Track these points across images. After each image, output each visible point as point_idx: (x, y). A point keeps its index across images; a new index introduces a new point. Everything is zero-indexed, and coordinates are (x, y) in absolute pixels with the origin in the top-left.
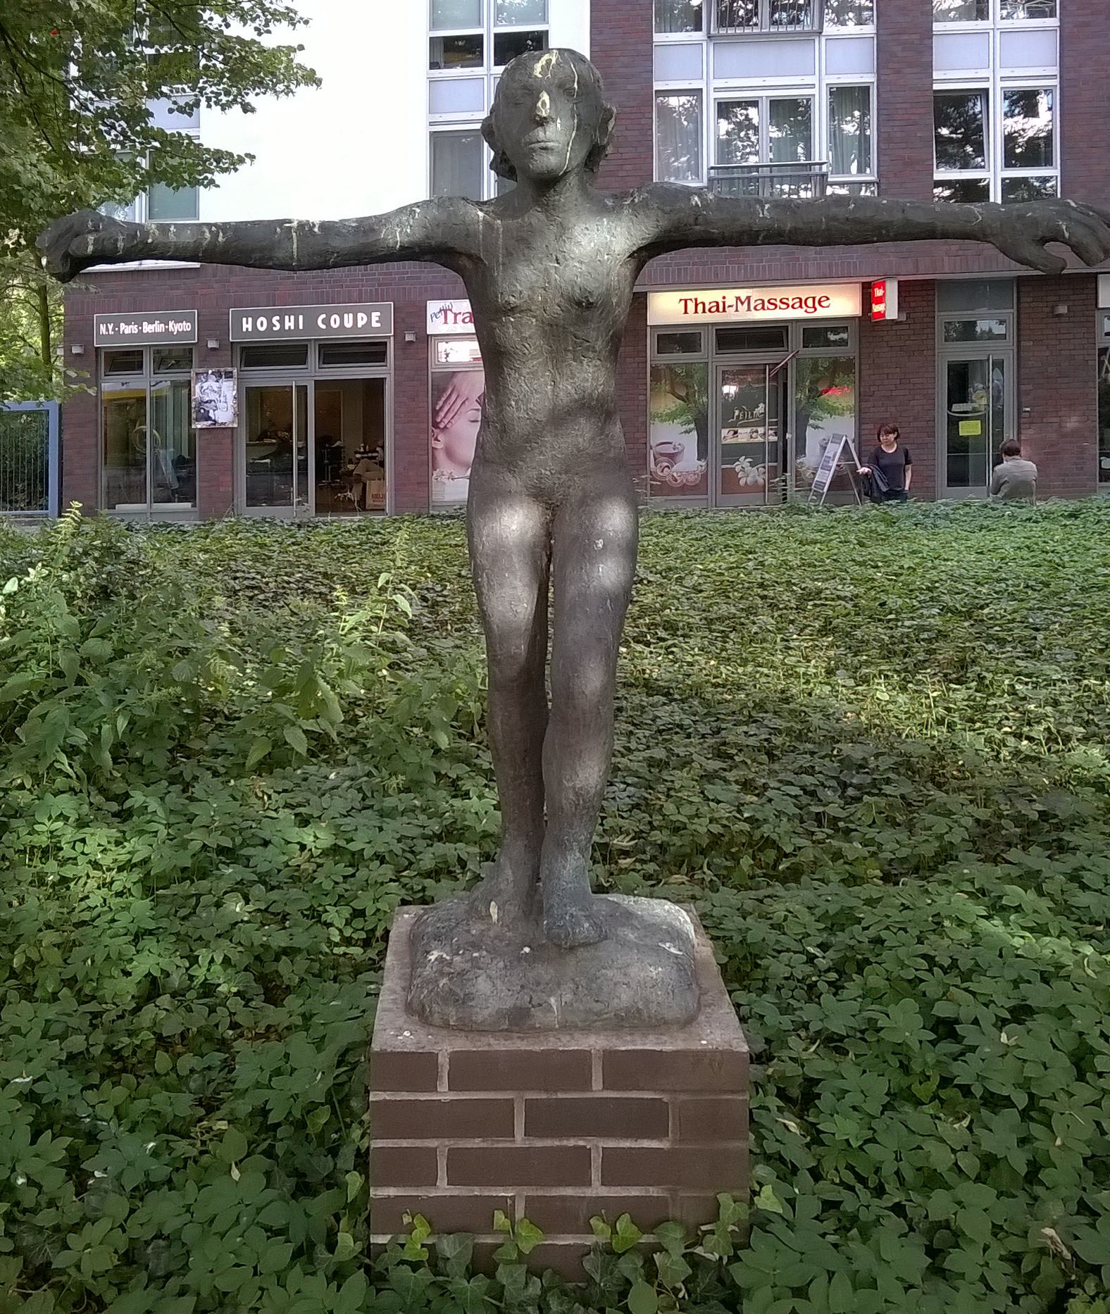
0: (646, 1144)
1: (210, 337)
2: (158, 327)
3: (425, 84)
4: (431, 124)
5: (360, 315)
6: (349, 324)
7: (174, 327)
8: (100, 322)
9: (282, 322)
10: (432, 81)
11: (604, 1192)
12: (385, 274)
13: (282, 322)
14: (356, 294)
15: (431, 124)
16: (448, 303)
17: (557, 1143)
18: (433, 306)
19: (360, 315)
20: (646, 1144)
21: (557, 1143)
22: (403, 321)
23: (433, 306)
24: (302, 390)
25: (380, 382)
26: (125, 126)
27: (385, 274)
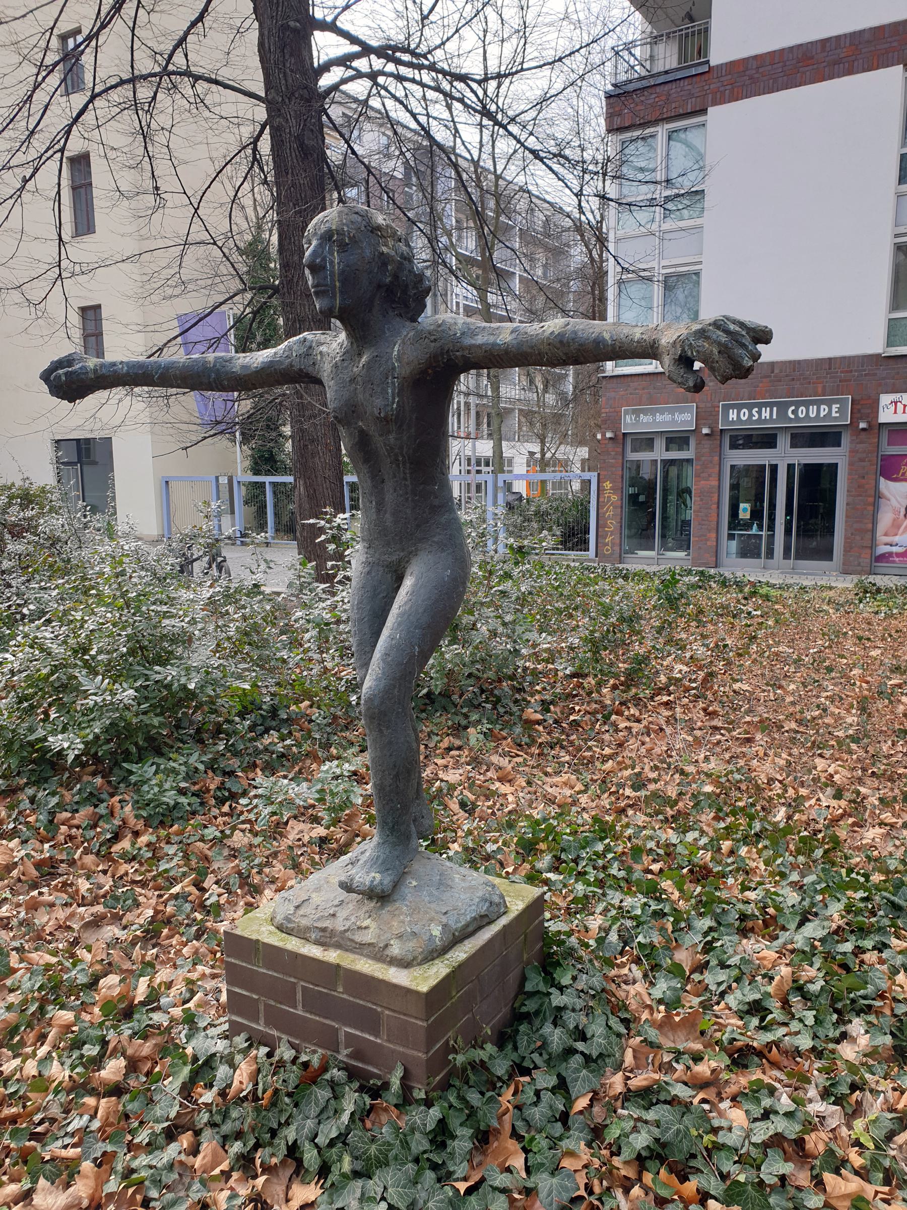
0: (367, 1036)
1: (705, 425)
2: (667, 417)
3: (892, 198)
4: (896, 236)
5: (822, 407)
6: (812, 415)
7: (679, 417)
8: (626, 412)
9: (760, 413)
10: (899, 196)
11: (300, 1013)
12: (847, 372)
13: (760, 413)
14: (820, 390)
15: (896, 236)
16: (898, 395)
17: (358, 1033)
18: (885, 399)
19: (822, 407)
20: (367, 1036)
21: (358, 1033)
22: (859, 411)
23: (885, 399)
24: (774, 469)
25: (833, 468)
26: (79, 851)
27: (847, 372)
